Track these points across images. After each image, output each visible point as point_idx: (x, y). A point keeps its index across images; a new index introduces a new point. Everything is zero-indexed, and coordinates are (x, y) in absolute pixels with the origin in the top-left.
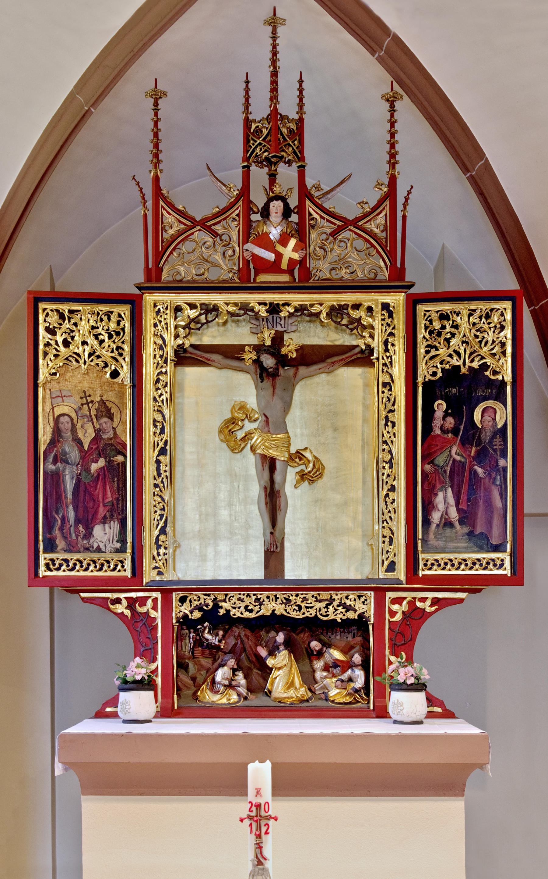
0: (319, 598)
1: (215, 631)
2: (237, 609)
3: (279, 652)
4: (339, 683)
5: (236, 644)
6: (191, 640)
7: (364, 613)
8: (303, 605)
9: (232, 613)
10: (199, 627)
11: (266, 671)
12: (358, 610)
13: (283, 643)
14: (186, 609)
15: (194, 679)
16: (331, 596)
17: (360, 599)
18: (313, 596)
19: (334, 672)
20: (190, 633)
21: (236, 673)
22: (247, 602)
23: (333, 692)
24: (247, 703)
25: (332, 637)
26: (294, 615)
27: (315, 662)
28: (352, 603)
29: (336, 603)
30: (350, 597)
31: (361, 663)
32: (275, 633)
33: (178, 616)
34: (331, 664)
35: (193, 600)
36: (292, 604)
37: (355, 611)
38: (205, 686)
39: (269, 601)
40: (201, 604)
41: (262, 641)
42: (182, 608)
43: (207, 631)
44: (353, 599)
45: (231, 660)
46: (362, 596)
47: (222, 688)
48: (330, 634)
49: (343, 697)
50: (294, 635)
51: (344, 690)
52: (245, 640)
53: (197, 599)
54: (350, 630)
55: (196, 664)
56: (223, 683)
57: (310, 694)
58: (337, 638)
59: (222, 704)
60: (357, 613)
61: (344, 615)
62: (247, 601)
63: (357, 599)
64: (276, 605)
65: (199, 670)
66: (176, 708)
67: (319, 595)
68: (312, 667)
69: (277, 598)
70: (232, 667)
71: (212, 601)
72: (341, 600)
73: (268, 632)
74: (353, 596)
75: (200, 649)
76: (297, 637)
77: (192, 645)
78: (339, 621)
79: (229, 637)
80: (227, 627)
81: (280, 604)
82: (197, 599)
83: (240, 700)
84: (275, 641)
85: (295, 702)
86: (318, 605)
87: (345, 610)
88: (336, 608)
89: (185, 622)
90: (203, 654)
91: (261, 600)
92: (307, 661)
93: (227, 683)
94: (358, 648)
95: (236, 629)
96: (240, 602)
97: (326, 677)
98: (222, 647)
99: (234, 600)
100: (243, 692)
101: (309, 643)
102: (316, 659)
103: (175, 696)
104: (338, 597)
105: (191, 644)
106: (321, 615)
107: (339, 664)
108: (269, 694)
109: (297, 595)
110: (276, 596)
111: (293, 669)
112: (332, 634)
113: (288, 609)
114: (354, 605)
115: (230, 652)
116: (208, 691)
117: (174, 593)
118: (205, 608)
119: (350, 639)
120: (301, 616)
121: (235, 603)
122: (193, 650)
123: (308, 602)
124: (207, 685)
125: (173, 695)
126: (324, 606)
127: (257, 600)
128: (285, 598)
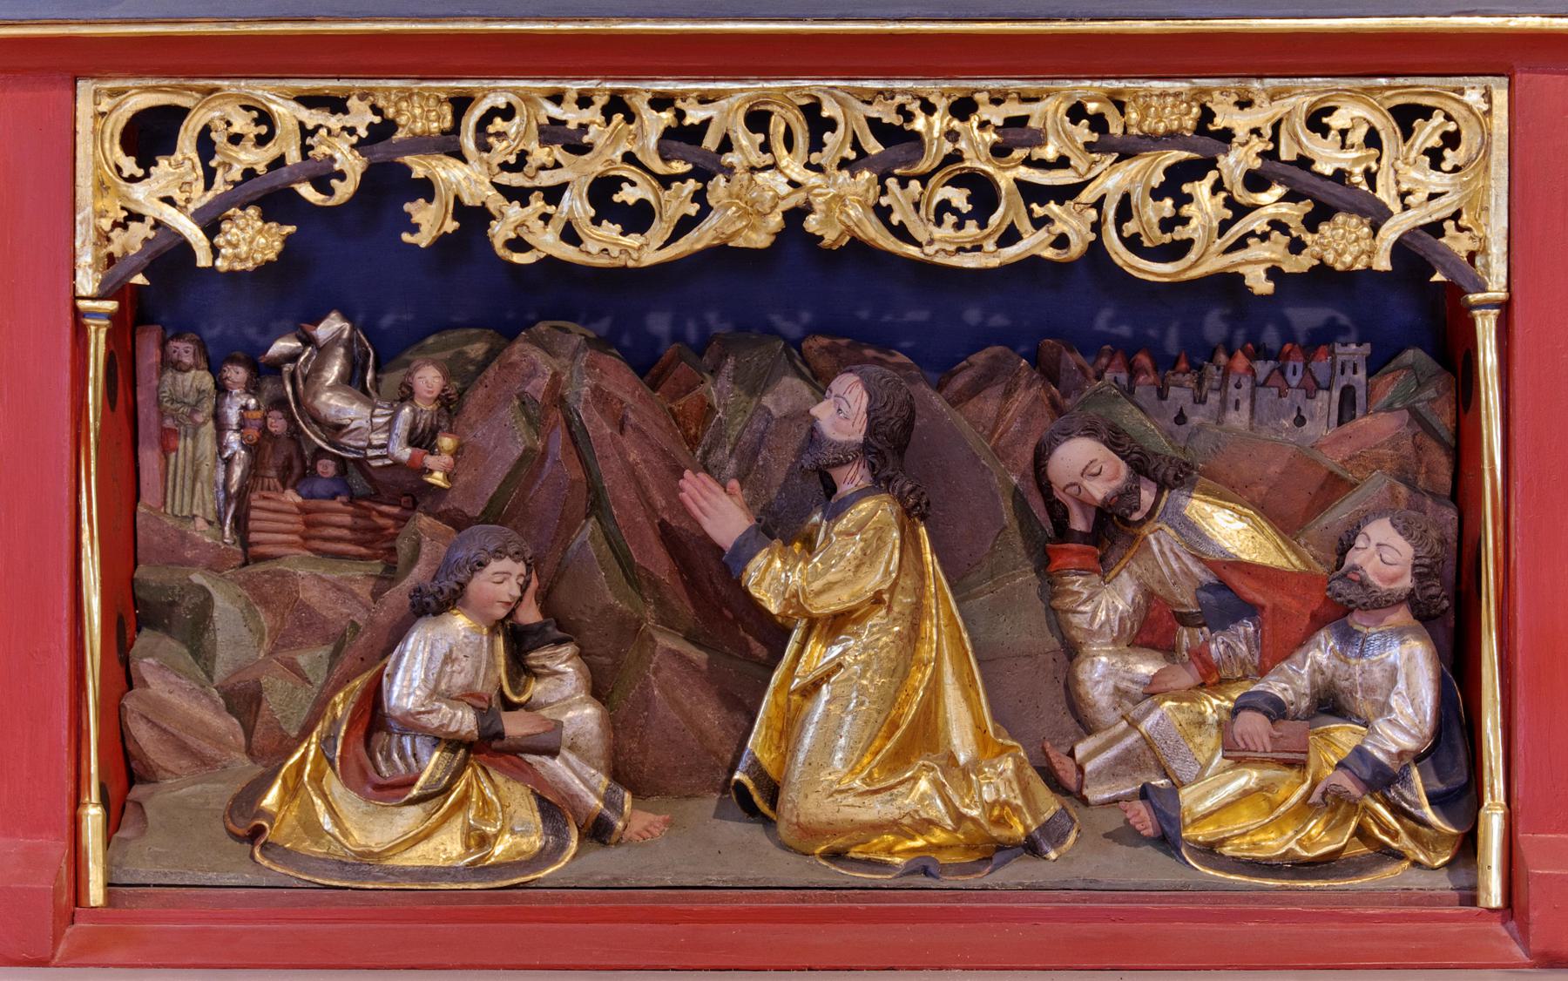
0: (1115, 129)
1: (392, 379)
2: (537, 204)
3: (834, 514)
4: (1254, 725)
5: (530, 462)
6: (233, 438)
7: (1436, 229)
8: (1005, 179)
9: (500, 232)
10: (283, 346)
11: (745, 644)
12: (1395, 207)
13: (865, 448)
14: (169, 195)
15: (243, 701)
16: (1207, 115)
17: (1407, 133)
18: (1076, 113)
19: (1216, 649)
20: (222, 389)
21: (536, 658)
22: (605, 157)
23: (1214, 794)
24: (604, 864)
25: (1194, 420)
26: (940, 244)
27: (1077, 583)
28: (1352, 160)
29: (1236, 162)
30: (1336, 121)
31: (1407, 583)
32: (806, 391)
33: (115, 248)
34: (1187, 600)
35: (219, 138)
36: (924, 166)
37: (1377, 216)
38: (312, 747)
39: (765, 147)
40: (278, 163)
41: (717, 443)
42: (143, 195)
43: (333, 371)
44: (1357, 136)
45: (495, 566)
46: (1427, 113)
47: (433, 763)
48: (1180, 395)
49: (1278, 824)
50: (937, 401)
51: (1292, 774)
52: (599, 426)
53: (252, 131)
54: (1320, 366)
55: (265, 602)
56: (434, 721)
57: (1050, 804)
58: (1236, 414)
59: (427, 873)
60: (1390, 233)
61: (1297, 246)
62: (609, 145)
63: (1388, 129)
64: (812, 178)
65: (282, 642)
66: (96, 893)
67: (1121, 107)
68: (1057, 620)
69: (819, 125)
70: (501, 612)
71: (360, 145)
72: (1275, 138)
73: (756, 385)
74: (1360, 111)
75: (292, 497)
76: (958, 419)
77: (237, 472)
78: (1261, 285)
79: (489, 409)
80: (477, 350)
81: (844, 164)
82: (252, 131)
83: (561, 848)
84: (814, 436)
85: (946, 858)
86: (1113, 179)
87: (1306, 207)
88: (1243, 196)
89: (163, 291)
90: (310, 527)
91: (711, 142)
92: (1025, 578)
93: (464, 721)
94: (1376, 485)
95: (537, 355)
96: (558, 152)
97: (1153, 691)
98: (437, 478)
99: (514, 135)
100: (578, 786)
101: (1041, 457)
102: (1082, 570)
103: (93, 814)
104: (1252, 115)
105: (228, 462)
106: (1133, 243)
107: (1250, 590)
108: (758, 802)
109: (963, 108)
110: (812, 111)
111: (930, 628)
112: (1200, 400)
113: (899, 200)
114: (1370, 177)
115: (494, 514)
116: (333, 784)
117: (85, 88)
118: (307, 191)
119: (1319, 428)
120: (992, 258)
121: (523, 156)
122: (240, 509)
123: (1038, 153)
124: (327, 742)
125: (78, 802)
126: (1158, 179)
127: (682, 136)
128: (875, 125)
